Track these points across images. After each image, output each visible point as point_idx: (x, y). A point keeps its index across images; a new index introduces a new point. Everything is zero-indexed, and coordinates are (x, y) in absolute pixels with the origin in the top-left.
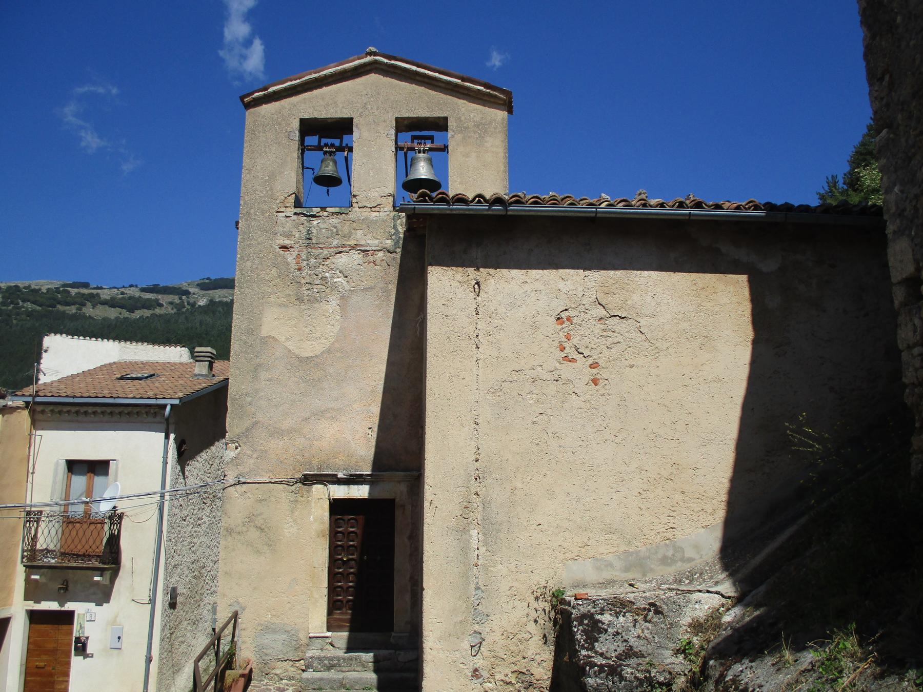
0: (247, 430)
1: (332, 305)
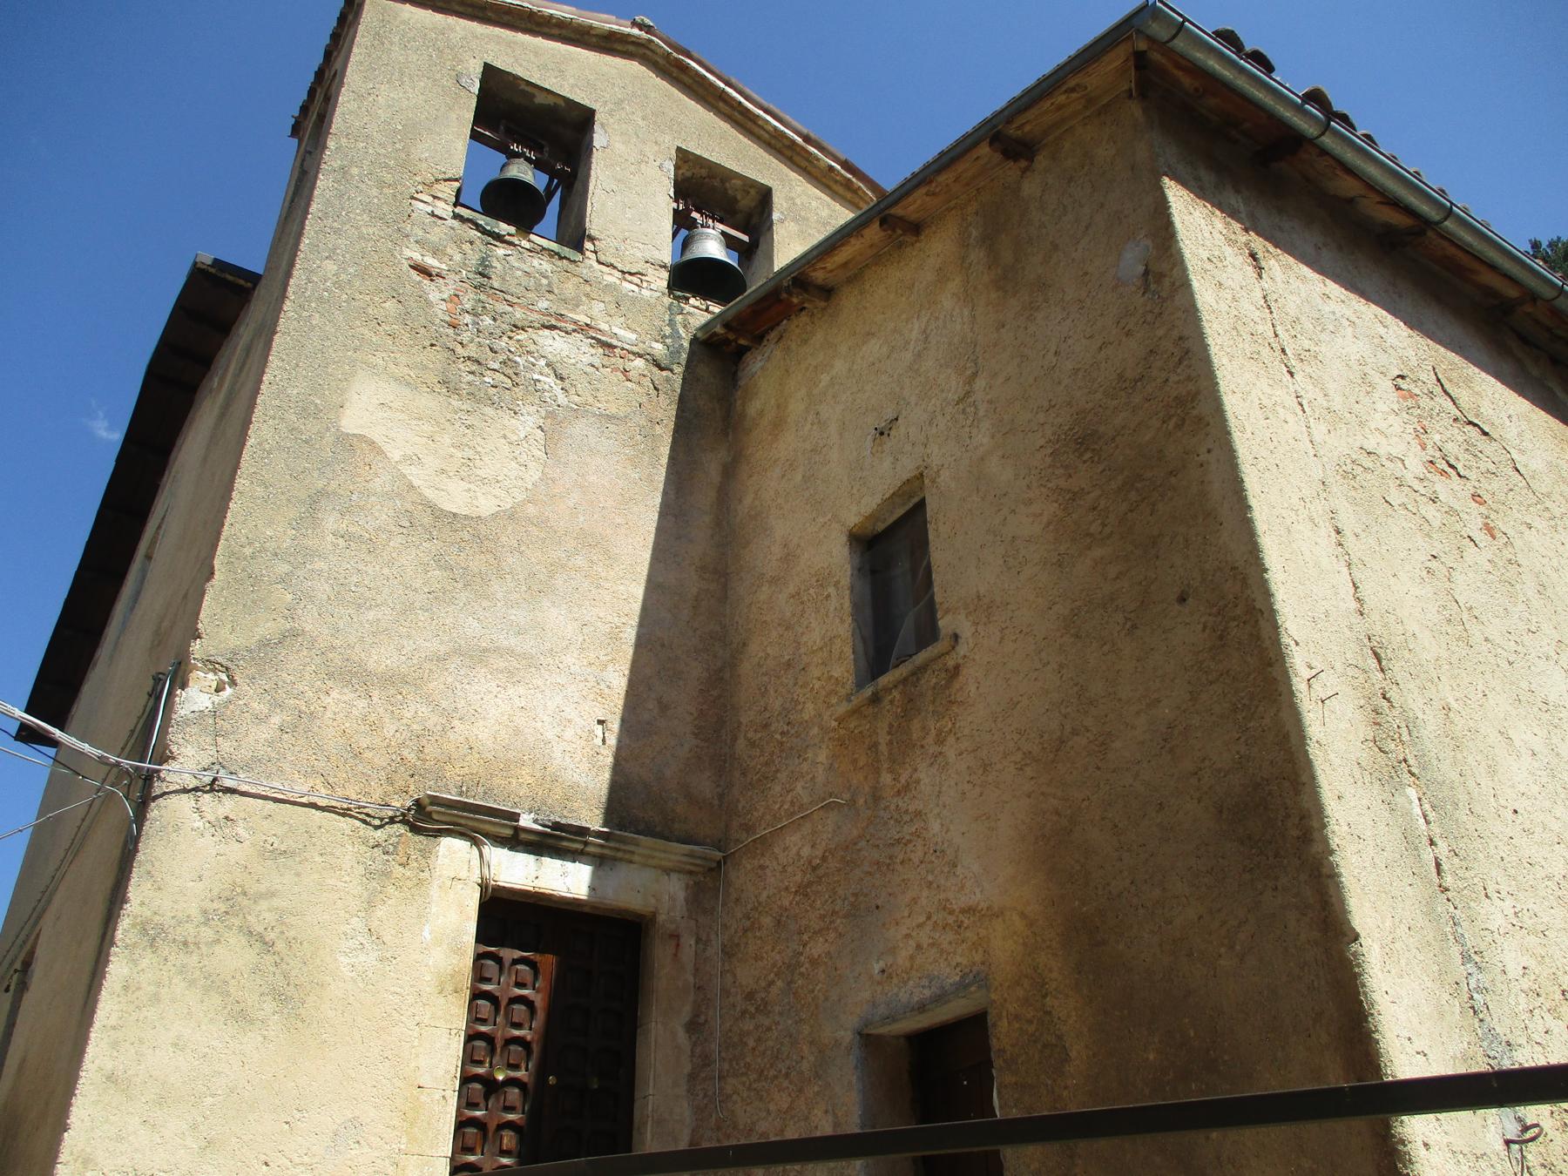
0: (264, 644)
1: (527, 422)
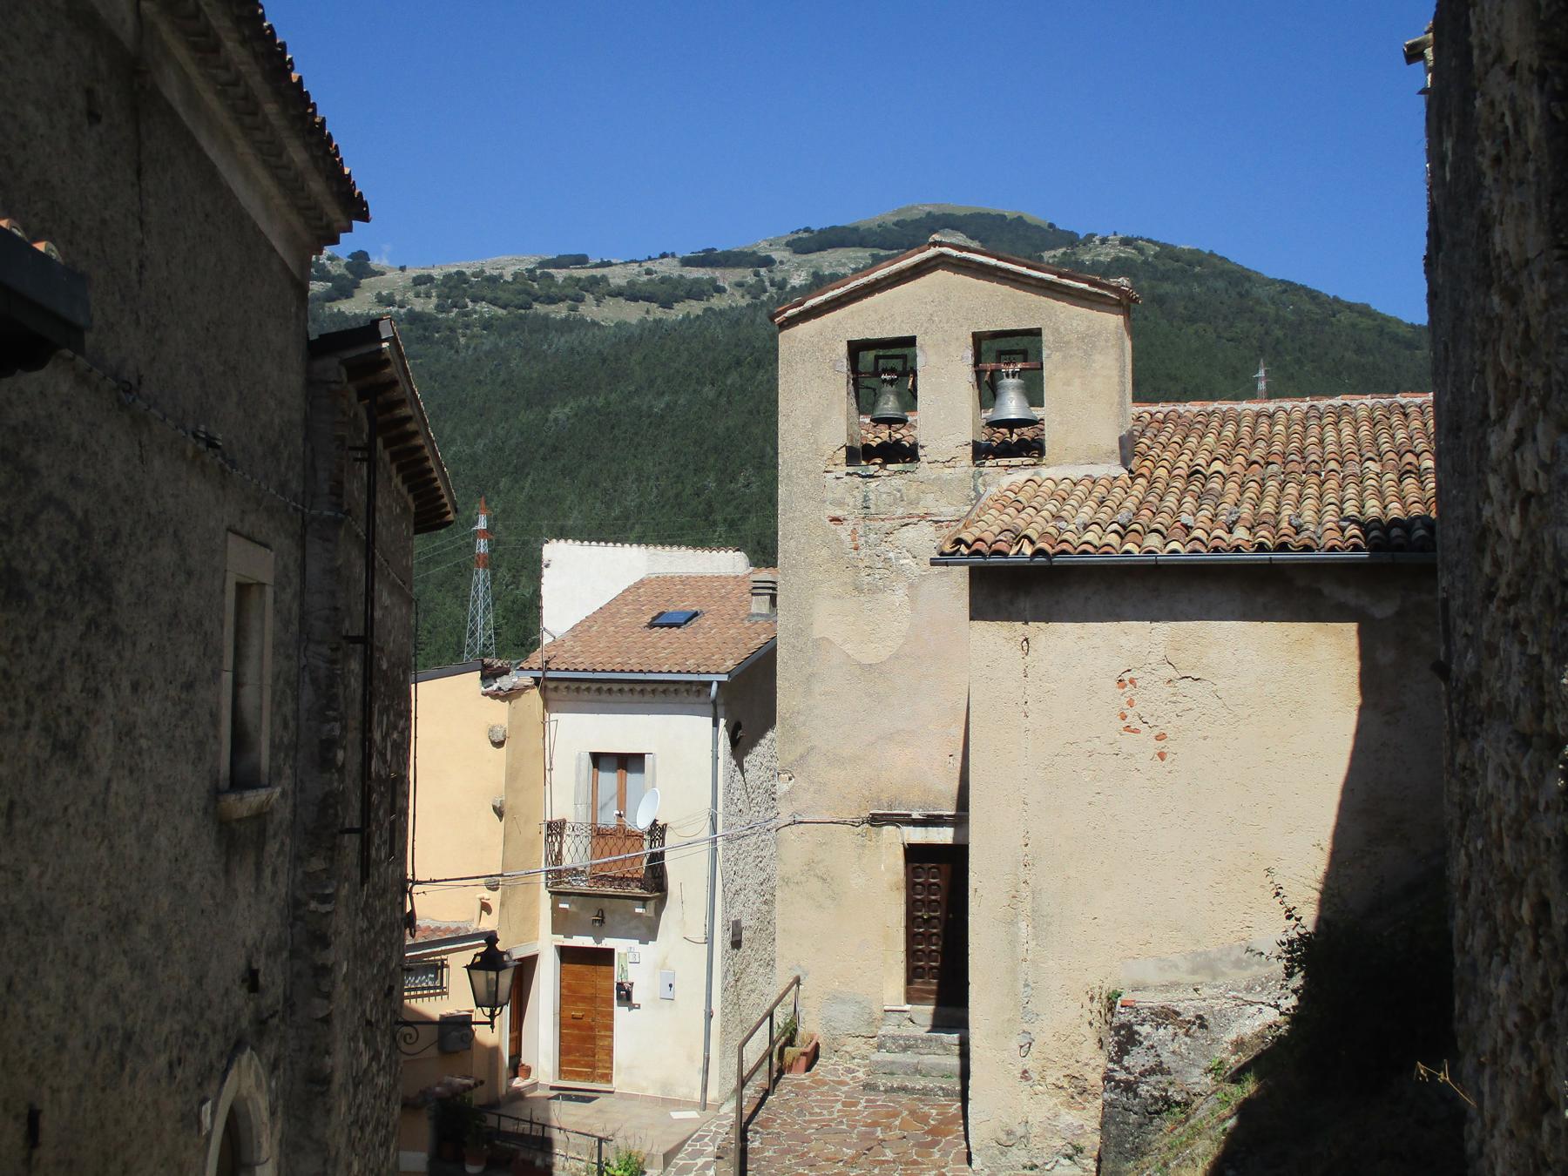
0: (802, 757)
1: (899, 596)
